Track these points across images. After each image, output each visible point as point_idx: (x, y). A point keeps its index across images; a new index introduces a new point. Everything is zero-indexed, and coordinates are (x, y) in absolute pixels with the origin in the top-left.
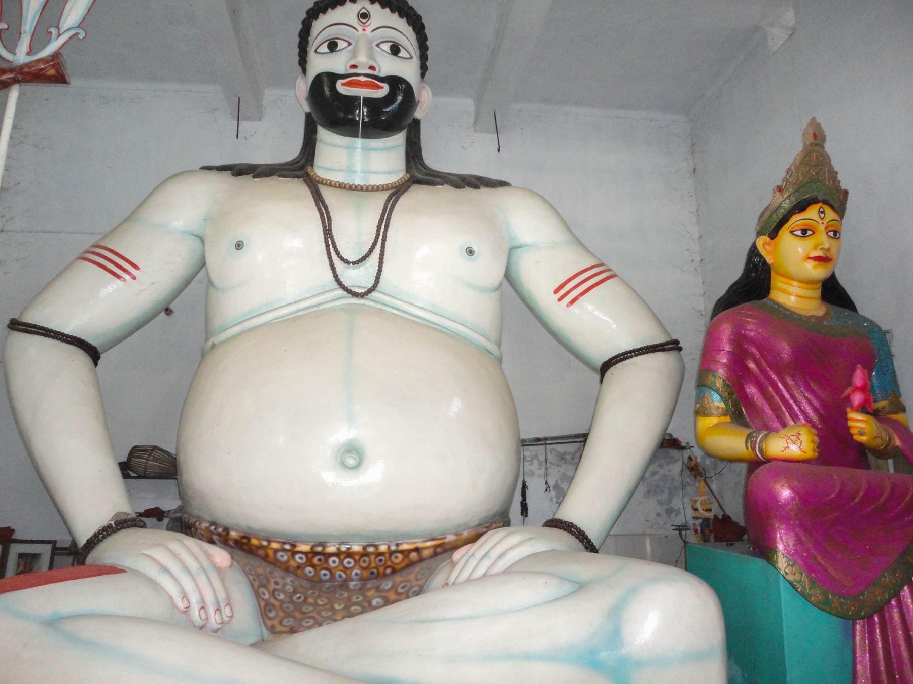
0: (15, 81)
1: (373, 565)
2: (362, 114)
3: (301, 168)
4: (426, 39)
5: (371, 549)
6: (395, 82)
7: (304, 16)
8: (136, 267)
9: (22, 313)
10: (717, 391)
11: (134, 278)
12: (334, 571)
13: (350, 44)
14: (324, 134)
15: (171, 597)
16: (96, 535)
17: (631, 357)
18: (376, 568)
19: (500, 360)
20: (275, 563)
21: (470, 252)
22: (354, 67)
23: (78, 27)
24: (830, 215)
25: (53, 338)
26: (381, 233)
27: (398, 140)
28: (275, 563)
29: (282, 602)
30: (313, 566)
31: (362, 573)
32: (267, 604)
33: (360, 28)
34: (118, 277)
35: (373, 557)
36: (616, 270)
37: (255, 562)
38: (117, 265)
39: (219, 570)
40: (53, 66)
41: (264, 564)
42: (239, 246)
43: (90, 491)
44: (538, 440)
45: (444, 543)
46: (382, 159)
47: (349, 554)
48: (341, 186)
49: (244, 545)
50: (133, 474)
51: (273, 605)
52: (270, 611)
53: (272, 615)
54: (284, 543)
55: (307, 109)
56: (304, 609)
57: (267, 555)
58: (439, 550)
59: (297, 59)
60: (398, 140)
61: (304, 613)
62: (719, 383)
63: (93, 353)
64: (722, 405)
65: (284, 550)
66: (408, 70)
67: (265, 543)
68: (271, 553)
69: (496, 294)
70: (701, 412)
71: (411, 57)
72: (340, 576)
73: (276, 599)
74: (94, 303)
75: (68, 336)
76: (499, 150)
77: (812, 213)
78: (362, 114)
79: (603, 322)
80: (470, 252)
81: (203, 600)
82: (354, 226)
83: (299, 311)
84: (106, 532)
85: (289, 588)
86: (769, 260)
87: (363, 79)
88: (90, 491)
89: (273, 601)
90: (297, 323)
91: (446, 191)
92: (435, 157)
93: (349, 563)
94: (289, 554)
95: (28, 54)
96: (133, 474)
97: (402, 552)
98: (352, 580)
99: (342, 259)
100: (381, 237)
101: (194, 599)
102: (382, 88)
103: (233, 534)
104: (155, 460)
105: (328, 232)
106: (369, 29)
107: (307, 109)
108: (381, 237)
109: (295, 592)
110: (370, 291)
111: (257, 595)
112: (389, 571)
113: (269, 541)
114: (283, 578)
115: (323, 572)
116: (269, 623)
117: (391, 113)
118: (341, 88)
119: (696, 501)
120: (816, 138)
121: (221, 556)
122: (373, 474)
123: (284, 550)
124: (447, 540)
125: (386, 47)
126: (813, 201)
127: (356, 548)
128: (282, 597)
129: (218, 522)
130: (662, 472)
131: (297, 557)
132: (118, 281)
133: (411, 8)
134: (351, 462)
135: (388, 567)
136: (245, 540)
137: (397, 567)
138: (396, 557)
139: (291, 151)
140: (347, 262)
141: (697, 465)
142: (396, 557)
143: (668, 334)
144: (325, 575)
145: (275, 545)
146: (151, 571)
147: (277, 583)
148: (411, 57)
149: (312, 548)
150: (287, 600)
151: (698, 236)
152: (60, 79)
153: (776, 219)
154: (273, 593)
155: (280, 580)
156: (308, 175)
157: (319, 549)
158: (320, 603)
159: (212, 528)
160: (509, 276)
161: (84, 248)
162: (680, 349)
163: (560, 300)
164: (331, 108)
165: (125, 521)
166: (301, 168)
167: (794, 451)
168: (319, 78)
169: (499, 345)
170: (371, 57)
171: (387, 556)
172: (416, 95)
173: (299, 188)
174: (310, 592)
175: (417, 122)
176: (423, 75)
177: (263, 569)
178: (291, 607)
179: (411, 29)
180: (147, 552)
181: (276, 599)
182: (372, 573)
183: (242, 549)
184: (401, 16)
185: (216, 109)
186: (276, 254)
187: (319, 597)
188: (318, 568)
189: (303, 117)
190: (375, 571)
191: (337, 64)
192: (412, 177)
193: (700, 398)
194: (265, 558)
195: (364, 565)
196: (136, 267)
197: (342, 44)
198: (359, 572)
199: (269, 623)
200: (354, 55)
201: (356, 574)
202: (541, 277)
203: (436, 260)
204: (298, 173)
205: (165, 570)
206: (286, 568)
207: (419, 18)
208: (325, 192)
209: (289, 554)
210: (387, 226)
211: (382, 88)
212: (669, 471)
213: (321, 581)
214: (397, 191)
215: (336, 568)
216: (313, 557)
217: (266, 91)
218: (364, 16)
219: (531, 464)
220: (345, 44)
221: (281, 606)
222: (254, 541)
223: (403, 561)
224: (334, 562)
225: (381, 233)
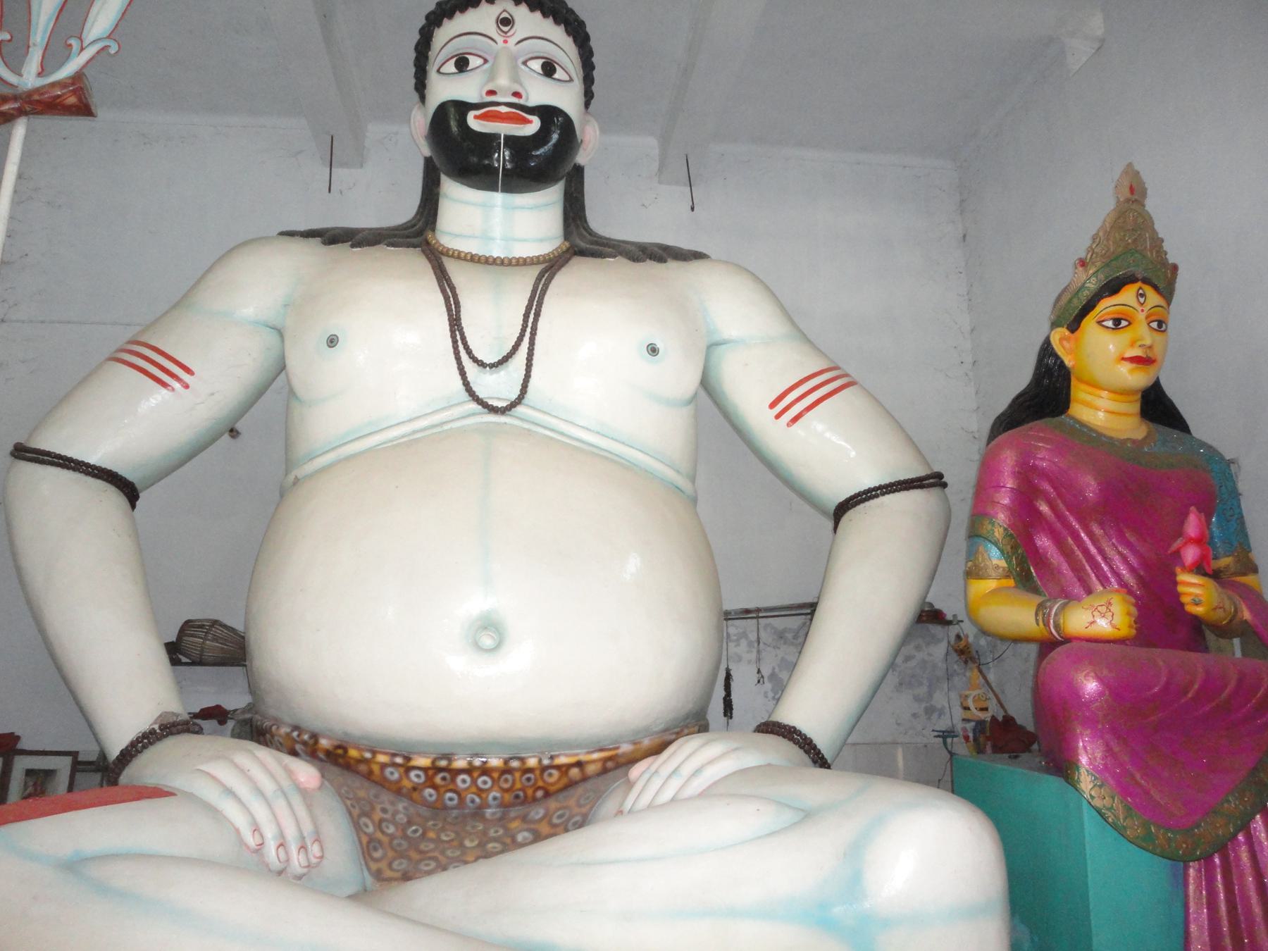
0: (21, 112)
1: (518, 786)
2: (502, 158)
3: (418, 233)
4: (591, 53)
5: (515, 764)
6: (548, 114)
9: (30, 435)
10: (996, 544)
11: (187, 387)
12: (463, 795)
13: (486, 61)
15: (237, 831)
16: (133, 744)
17: (877, 496)
19: (694, 501)
20: (383, 783)
21: (653, 350)
23: (109, 37)
24: (1153, 298)
25: (74, 469)
26: (530, 325)
28: (383, 783)
29: (392, 837)
30: (435, 787)
32: (371, 840)
33: (500, 39)
34: (164, 385)
35: (517, 775)
36: (855, 375)
37: (356, 782)
38: (163, 369)
40: (74, 92)
41: (367, 784)
42: (332, 341)
43: (126, 685)
45: (616, 756)
47: (485, 770)
48: (474, 259)
49: (339, 757)
50: (184, 660)
51: (380, 842)
52: (375, 849)
53: (377, 855)
54: (394, 755)
55: (427, 152)
56: (422, 847)
57: (371, 772)
58: (610, 764)
59: (412, 81)
61: (421, 852)
62: (998, 533)
63: (130, 491)
64: (1003, 563)
65: (395, 765)
66: (566, 97)
67: (368, 755)
68: (376, 768)
70: (974, 572)
71: (571, 80)
72: (473, 801)
73: (383, 832)
74: (131, 422)
75: (94, 467)
76: (693, 209)
77: (1127, 296)
78: (502, 158)
79: (836, 449)
80: (653, 350)
82: (492, 315)
83: (414, 432)
84: (147, 740)
85: (401, 818)
86: (1068, 362)
87: (504, 109)
88: (126, 685)
89: (379, 835)
90: (413, 449)
91: (619, 266)
92: (604, 219)
93: (485, 783)
94: (402, 770)
95: (39, 75)
96: (184, 660)
97: (558, 767)
98: (489, 806)
99: (475, 360)
100: (529, 330)
101: (269, 832)
103: (324, 743)
104: (215, 639)
105: (455, 323)
106: (512, 41)
107: (427, 152)
108: (529, 330)
109: (410, 823)
110: (513, 405)
112: (540, 794)
113: (374, 753)
114: (392, 803)
115: (449, 795)
116: (374, 866)
117: (542, 157)
118: (474, 122)
120: (1134, 193)
121: (306, 773)
122: (518, 659)
123: (395, 765)
124: (620, 751)
125: (536, 65)
126: (1130, 280)
127: (495, 762)
128: (391, 830)
130: (919, 656)
131: (413, 774)
132: (164, 391)
133: (572, 12)
134: (487, 642)
135: (539, 788)
136: (340, 751)
137: (552, 789)
138: (550, 775)
139: (405, 209)
140: (481, 364)
141: (967, 646)
142: (550, 775)
143: (927, 464)
144: (451, 799)
145: (382, 758)
146: (210, 793)
147: (384, 811)
148: (571, 80)
150: (399, 834)
152: (84, 110)
153: (1078, 304)
154: (379, 825)
155: (388, 807)
156: (428, 243)
157: (443, 763)
159: (295, 734)
161: (120, 343)
162: (945, 485)
163: (778, 417)
164: (461, 151)
165: (174, 725)
166: (418, 233)
167: (1103, 626)
168: (443, 108)
169: (693, 479)
170: (516, 79)
171: (538, 772)
174: (431, 823)
175: (579, 170)
176: (587, 105)
177: (365, 791)
178: (405, 844)
180: (203, 768)
181: (383, 832)
182: (517, 797)
183: (336, 764)
184: (557, 22)
185: (301, 152)
186: (383, 352)
187: (443, 829)
188: (442, 790)
190: (521, 794)
191: (467, 89)
192: (572, 246)
193: (972, 554)
194: (369, 776)
195: (506, 786)
197: (474, 62)
198: (498, 795)
199: (374, 866)
200: (492, 76)
201: (495, 798)
202: (752, 386)
203: (607, 361)
205: (230, 792)
206: (398, 791)
207: (582, 24)
208: (451, 266)
209: (402, 770)
210: (537, 315)
212: (930, 655)
213: (445, 808)
214: (550, 267)
216: (435, 774)
218: (506, 22)
220: (479, 61)
221: (390, 843)
222: (353, 753)
223: (559, 779)
224: (464, 781)
225: (530, 325)
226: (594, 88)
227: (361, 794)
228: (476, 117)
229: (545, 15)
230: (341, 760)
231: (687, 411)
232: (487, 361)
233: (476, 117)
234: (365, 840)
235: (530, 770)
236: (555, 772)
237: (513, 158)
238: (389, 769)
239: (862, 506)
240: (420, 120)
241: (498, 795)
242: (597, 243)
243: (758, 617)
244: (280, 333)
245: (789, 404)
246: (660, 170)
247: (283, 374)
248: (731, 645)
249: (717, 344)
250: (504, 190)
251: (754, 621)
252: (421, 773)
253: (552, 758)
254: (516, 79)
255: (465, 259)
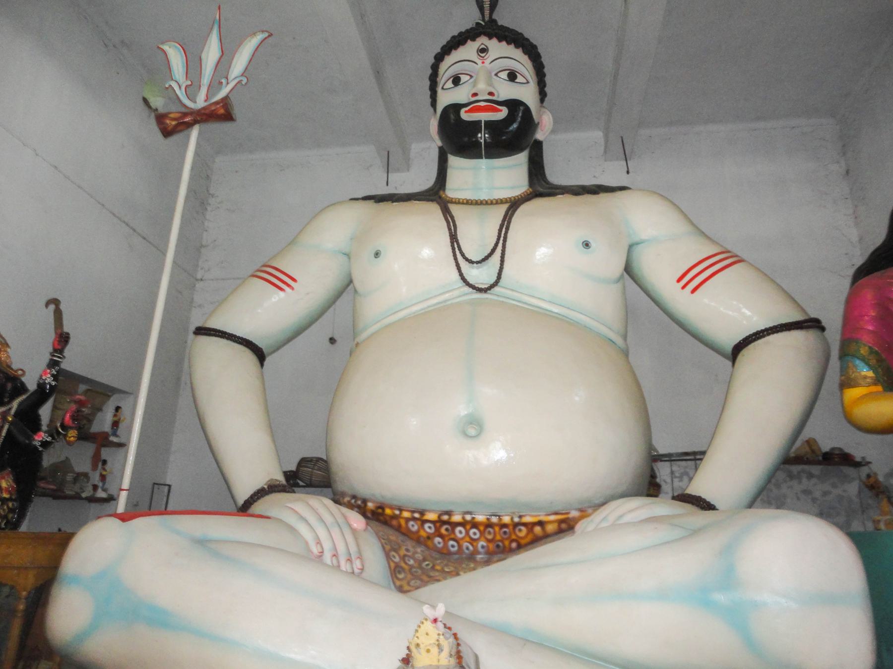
0: (195, 122)
1: (498, 537)
2: (483, 137)
3: (435, 193)
4: (544, 75)
5: (494, 520)
6: (514, 105)
7: (433, 61)
8: (294, 280)
9: (206, 321)
10: (863, 359)
11: (293, 289)
12: (461, 542)
13: (471, 77)
14: (454, 161)
15: (307, 543)
16: (252, 497)
17: (764, 336)
18: (502, 541)
19: (626, 353)
20: (406, 534)
21: (587, 245)
22: (475, 95)
23: (242, 75)
25: (228, 339)
26: (502, 235)
27: (522, 158)
28: (406, 534)
29: (411, 567)
30: (441, 536)
31: (488, 546)
32: (397, 566)
33: (479, 62)
34: (281, 289)
35: (497, 529)
36: (744, 256)
37: (390, 532)
38: (277, 278)
39: (354, 531)
40: (223, 107)
41: (397, 533)
42: (377, 254)
44: (686, 454)
45: (568, 518)
46: (506, 175)
47: (475, 525)
48: (469, 203)
49: (378, 515)
50: (301, 483)
51: (401, 567)
52: (400, 572)
53: (401, 576)
54: (413, 512)
55: (440, 143)
56: (432, 574)
57: (400, 526)
58: (564, 526)
60: (522, 158)
61: (430, 577)
62: (864, 351)
63: (260, 355)
64: (871, 374)
65: (414, 519)
66: (527, 93)
67: (397, 512)
68: (403, 522)
69: (619, 286)
70: (846, 383)
71: (528, 82)
72: (468, 548)
73: (406, 563)
74: (261, 312)
75: (239, 338)
76: (628, 172)
78: (483, 137)
79: (730, 307)
80: (587, 245)
81: (335, 548)
82: (477, 232)
83: (429, 307)
84: (260, 494)
85: (419, 556)
87: (482, 104)
89: (403, 565)
90: (427, 322)
92: (555, 175)
93: (475, 534)
94: (419, 523)
95: (206, 101)
96: (301, 483)
97: (525, 524)
98: (479, 553)
99: (467, 260)
100: (502, 239)
101: (327, 546)
102: (501, 111)
103: (370, 505)
104: (319, 470)
105: (454, 238)
106: (487, 62)
107: (440, 143)
108: (502, 239)
109: (424, 560)
110: (492, 286)
111: (388, 556)
112: (514, 545)
113: (401, 510)
114: (413, 547)
115: (451, 543)
116: (398, 583)
117: (512, 133)
118: (465, 115)
119: (879, 521)
121: (357, 520)
122: (495, 452)
123: (414, 519)
124: (571, 516)
125: (504, 75)
127: (480, 518)
128: (412, 562)
129: (359, 496)
130: (836, 492)
131: (427, 526)
132: (281, 294)
133: (527, 40)
134: (472, 432)
135: (513, 541)
136: (380, 511)
137: (523, 542)
138: (520, 530)
140: (471, 262)
141: (877, 481)
142: (520, 530)
143: (803, 310)
144: (453, 546)
145: (406, 514)
146: (292, 520)
147: (407, 550)
148: (528, 82)
149: (439, 517)
150: (416, 565)
151: (857, 239)
152: (228, 117)
154: (403, 558)
155: (411, 549)
156: (440, 197)
157: (445, 518)
158: (446, 570)
159: (353, 501)
160: (628, 269)
161: (257, 267)
162: (823, 329)
163: (683, 288)
164: (460, 136)
165: (276, 486)
166: (435, 193)
168: (446, 110)
169: (625, 337)
170: (490, 84)
171: (511, 527)
172: (535, 117)
173: (434, 209)
174: (438, 562)
175: (538, 145)
176: (542, 100)
177: (394, 536)
178: (420, 571)
179: (526, 57)
180: (289, 505)
181: (406, 563)
182: (498, 546)
183: (378, 520)
184: (517, 47)
185: (371, 166)
186: (412, 261)
187: (447, 565)
188: (447, 538)
189: (437, 150)
190: (500, 544)
191: (460, 95)
192: (534, 191)
193: (844, 370)
194: (398, 529)
195: (490, 537)
196: (294, 280)
197: (464, 78)
198: (484, 544)
199: (398, 583)
200: (475, 84)
201: (483, 547)
203: (556, 258)
204: (432, 198)
206: (418, 540)
207: (534, 47)
208: (453, 208)
209: (419, 523)
210: (507, 229)
211: (501, 111)
212: (844, 491)
213: (450, 553)
214: (514, 205)
215: (462, 539)
216: (441, 526)
217: (414, 146)
218: (483, 50)
219: (681, 480)
220: (468, 77)
221: (410, 570)
222: (388, 511)
223: (527, 534)
224: (460, 532)
225: (502, 235)
226: (546, 89)
227: (393, 538)
228: (466, 112)
229: (509, 43)
230: (381, 518)
231: (616, 288)
232: (474, 259)
233: (466, 112)
234: (392, 565)
235: (505, 526)
236: (523, 528)
237: (491, 136)
238: (411, 523)
239: (753, 344)
240: (434, 125)
241: (484, 544)
242: (552, 188)
243: (696, 460)
244: (348, 255)
245: (692, 278)
246: (605, 152)
247: (351, 286)
248: (676, 480)
249: (637, 244)
250: (486, 158)
251: (693, 462)
252: (432, 525)
253: (520, 517)
254: (490, 84)
255: (463, 203)
